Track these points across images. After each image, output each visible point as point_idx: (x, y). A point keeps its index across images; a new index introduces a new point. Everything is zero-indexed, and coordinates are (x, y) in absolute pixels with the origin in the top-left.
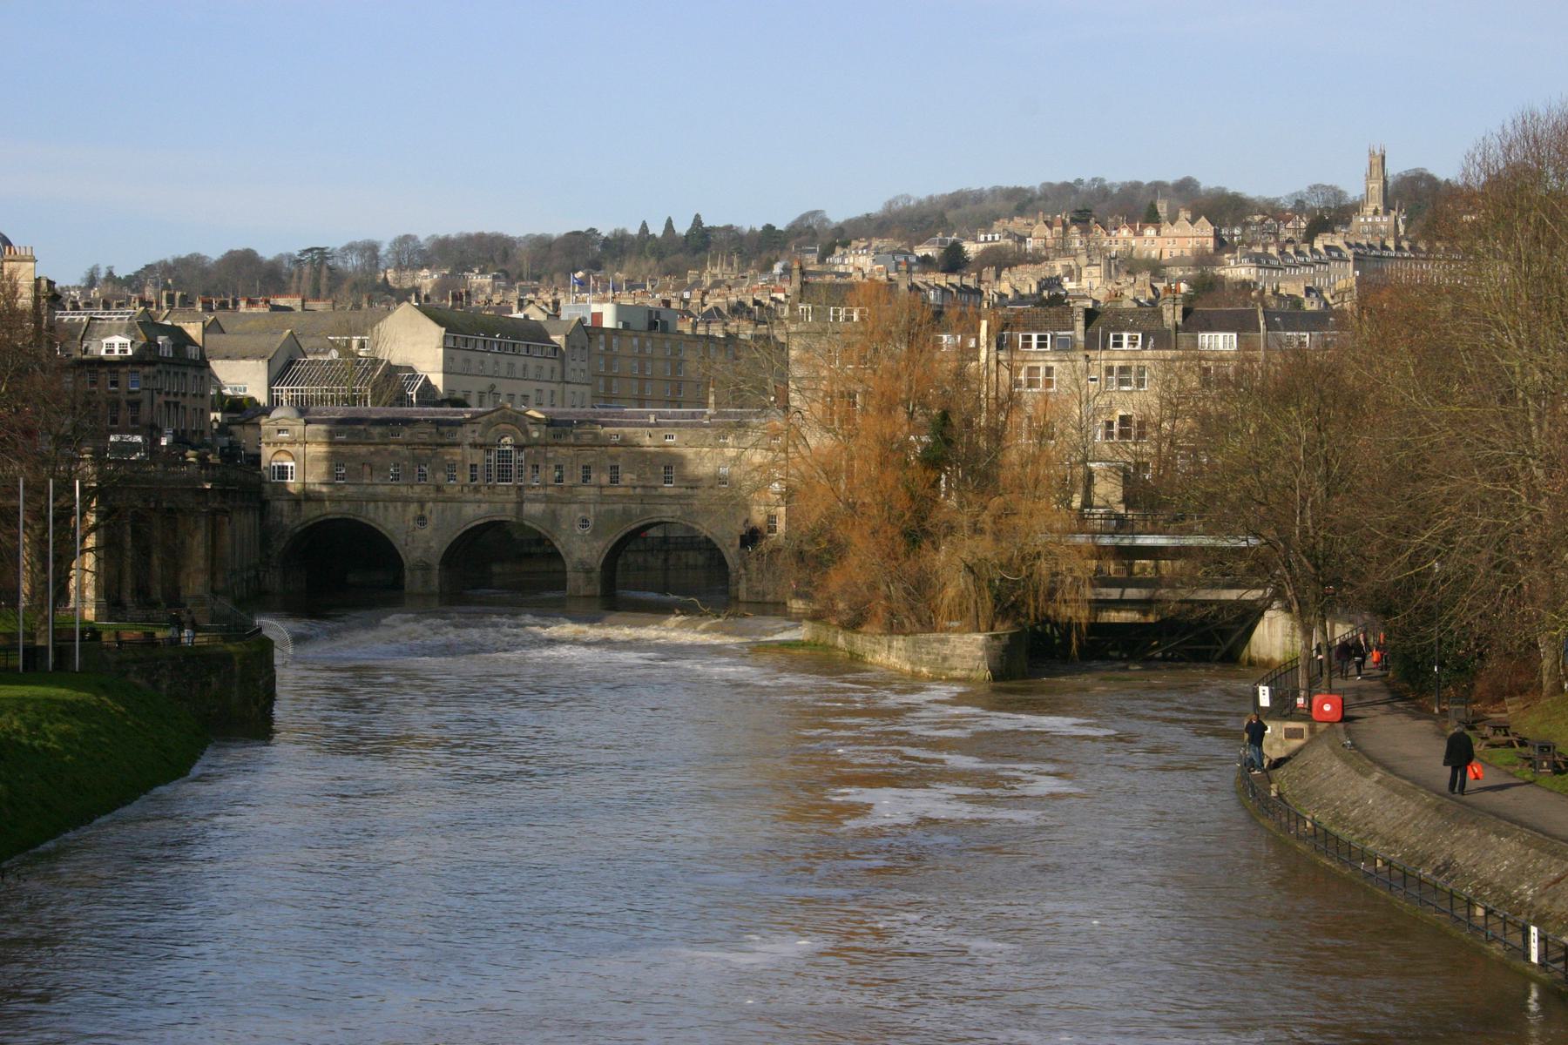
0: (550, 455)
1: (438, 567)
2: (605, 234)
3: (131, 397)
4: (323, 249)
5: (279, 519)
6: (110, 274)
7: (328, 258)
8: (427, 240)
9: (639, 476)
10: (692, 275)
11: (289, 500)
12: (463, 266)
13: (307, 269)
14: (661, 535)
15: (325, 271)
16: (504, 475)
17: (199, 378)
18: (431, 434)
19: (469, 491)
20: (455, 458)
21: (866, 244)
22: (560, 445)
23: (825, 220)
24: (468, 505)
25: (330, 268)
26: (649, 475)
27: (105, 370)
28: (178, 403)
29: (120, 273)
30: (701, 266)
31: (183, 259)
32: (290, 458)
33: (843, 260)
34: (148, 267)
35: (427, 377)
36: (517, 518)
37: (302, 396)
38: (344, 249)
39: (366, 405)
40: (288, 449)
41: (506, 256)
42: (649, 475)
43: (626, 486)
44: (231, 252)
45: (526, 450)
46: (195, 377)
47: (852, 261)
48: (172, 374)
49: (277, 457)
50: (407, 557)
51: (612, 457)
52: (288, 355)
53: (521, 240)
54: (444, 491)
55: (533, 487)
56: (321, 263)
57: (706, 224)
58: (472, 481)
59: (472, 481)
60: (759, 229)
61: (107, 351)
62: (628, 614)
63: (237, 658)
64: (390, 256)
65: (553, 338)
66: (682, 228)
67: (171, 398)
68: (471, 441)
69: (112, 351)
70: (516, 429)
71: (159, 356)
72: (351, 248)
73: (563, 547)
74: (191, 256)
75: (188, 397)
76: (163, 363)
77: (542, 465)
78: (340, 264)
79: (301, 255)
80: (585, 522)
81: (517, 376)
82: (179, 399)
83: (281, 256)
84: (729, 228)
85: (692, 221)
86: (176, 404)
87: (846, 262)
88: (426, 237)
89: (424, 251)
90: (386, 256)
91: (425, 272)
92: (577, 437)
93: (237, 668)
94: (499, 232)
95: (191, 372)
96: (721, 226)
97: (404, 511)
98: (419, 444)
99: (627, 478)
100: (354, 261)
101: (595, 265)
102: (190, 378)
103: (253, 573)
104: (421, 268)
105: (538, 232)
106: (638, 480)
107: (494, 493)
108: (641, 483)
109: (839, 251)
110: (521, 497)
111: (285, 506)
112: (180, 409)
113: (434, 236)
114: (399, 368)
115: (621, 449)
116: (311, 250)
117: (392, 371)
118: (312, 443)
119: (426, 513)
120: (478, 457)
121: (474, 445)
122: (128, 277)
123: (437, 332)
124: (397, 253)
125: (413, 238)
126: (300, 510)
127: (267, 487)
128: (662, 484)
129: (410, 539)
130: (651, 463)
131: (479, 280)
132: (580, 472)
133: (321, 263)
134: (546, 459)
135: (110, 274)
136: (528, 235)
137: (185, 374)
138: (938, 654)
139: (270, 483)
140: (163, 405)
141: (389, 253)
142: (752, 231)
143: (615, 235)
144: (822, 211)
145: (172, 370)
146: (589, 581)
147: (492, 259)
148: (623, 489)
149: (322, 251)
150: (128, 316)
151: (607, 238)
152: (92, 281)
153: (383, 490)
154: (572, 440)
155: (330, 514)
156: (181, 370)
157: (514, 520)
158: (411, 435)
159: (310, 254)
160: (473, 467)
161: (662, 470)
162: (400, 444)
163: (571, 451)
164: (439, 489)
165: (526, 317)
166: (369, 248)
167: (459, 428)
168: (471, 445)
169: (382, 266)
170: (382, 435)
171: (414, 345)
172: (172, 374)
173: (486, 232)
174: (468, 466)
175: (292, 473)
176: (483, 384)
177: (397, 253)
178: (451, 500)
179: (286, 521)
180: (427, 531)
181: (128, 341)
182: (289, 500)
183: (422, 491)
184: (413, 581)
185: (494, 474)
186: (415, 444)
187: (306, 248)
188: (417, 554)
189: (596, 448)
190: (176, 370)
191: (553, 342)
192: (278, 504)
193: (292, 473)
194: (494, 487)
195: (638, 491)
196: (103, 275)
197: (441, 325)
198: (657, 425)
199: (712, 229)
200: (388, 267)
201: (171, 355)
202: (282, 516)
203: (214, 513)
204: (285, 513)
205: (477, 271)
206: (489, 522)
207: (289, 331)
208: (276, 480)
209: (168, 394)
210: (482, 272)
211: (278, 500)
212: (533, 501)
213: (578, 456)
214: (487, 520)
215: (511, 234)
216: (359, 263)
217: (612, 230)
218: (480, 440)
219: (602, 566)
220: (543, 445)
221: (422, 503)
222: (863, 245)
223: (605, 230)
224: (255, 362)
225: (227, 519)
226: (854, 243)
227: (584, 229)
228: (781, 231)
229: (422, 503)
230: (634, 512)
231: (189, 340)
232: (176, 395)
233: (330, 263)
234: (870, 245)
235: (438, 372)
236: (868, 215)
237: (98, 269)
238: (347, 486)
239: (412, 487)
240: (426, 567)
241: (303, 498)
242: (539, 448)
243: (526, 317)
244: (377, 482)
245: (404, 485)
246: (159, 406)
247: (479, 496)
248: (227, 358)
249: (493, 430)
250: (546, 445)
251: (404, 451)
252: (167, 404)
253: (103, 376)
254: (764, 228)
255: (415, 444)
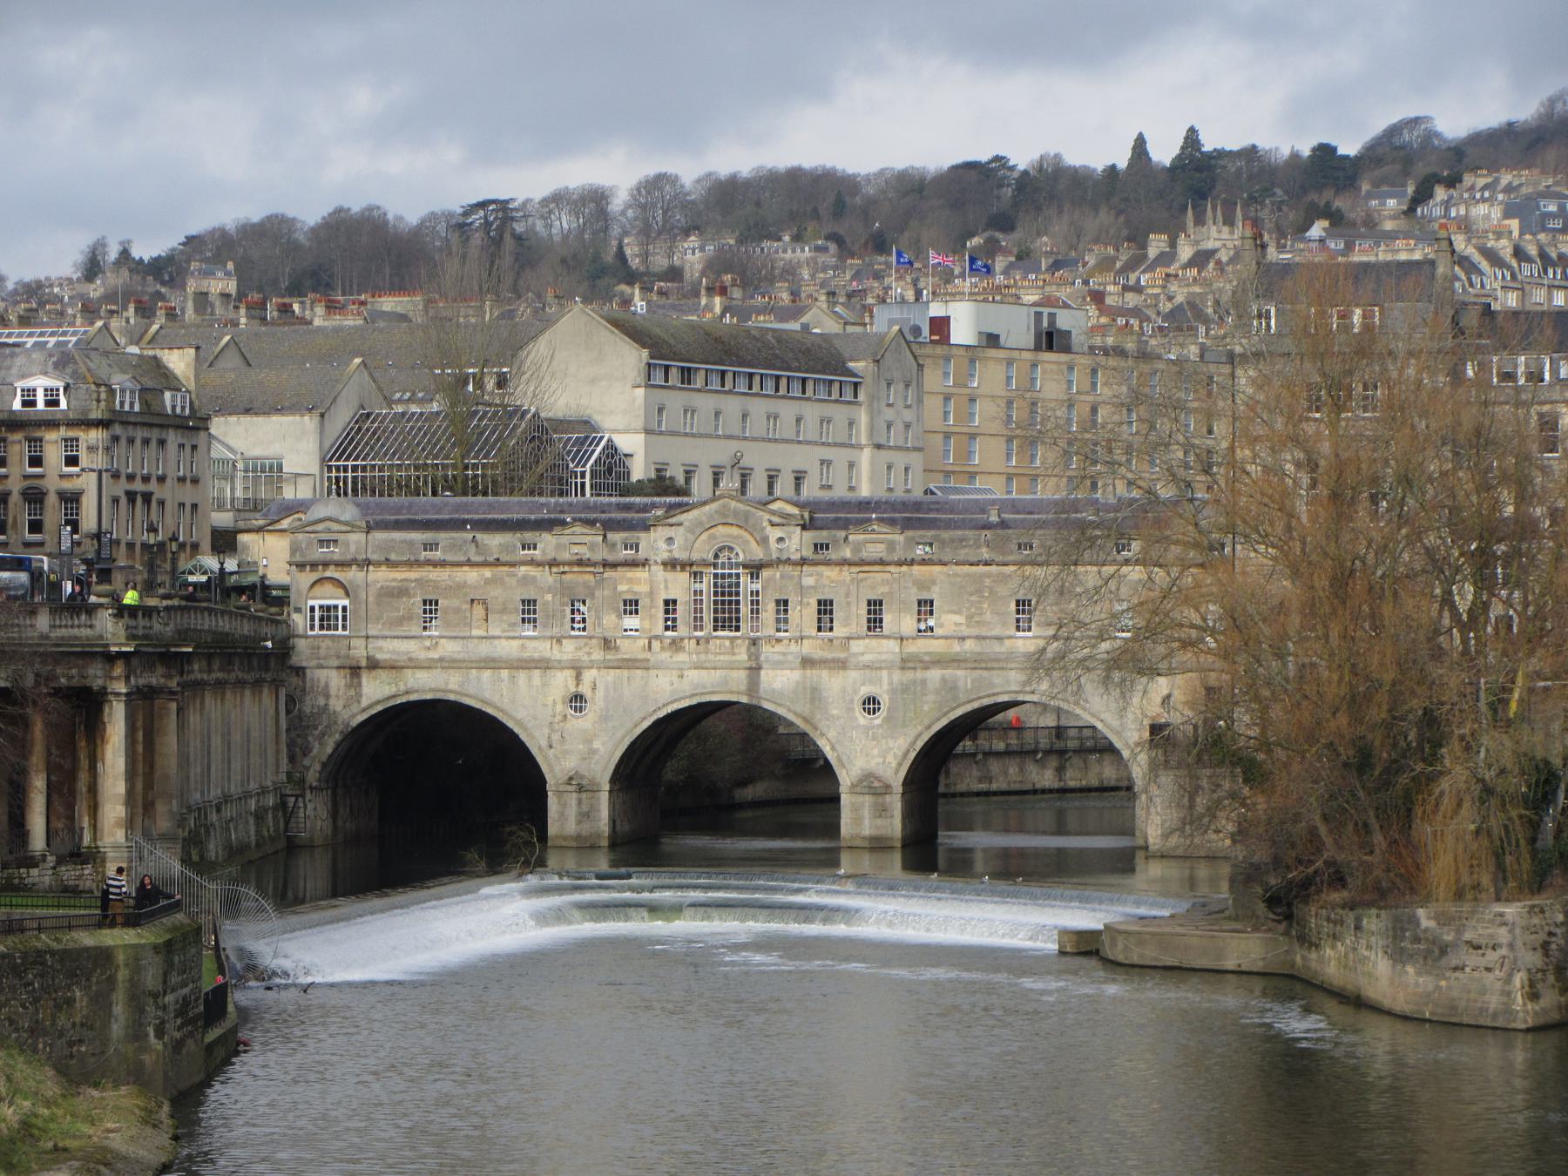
0: (808, 581)
1: (607, 787)
2: (1021, 167)
3: (67, 485)
4: (507, 202)
5: (321, 701)
6: (125, 254)
7: (513, 219)
8: (698, 181)
9: (969, 618)
10: (1156, 244)
11: (338, 668)
12: (759, 231)
13: (477, 239)
14: (1053, 724)
15: (508, 240)
16: (727, 617)
17: (188, 449)
18: (592, 547)
19: (662, 649)
20: (637, 588)
21: (1489, 180)
22: (828, 563)
23: (1431, 135)
24: (660, 673)
25: (518, 238)
26: (988, 616)
27: (18, 436)
28: (151, 494)
29: (144, 251)
30: (1174, 231)
31: (253, 226)
32: (341, 592)
33: (1447, 209)
34: (190, 240)
35: (610, 440)
36: (750, 696)
37: (355, 478)
38: (545, 202)
39: (583, 494)
40: (336, 575)
41: (839, 209)
42: (988, 616)
43: (946, 638)
44: (339, 210)
45: (765, 573)
46: (182, 446)
47: (1463, 212)
48: (138, 442)
49: (318, 590)
50: (552, 770)
51: (922, 585)
52: (356, 404)
53: (867, 178)
54: (616, 649)
55: (779, 640)
56: (501, 230)
57: (1208, 147)
58: (667, 628)
59: (667, 628)
60: (1306, 152)
61: (25, 404)
62: (445, 880)
63: (121, 958)
64: (630, 213)
65: (851, 365)
66: (1164, 152)
67: (138, 486)
68: (665, 556)
69: (33, 403)
70: (746, 535)
71: (114, 411)
72: (557, 199)
73: (833, 748)
74: (269, 218)
75: (169, 481)
76: (122, 423)
77: (793, 601)
78: (539, 226)
79: (466, 214)
80: (871, 704)
81: (785, 436)
82: (153, 486)
83: (433, 216)
84: (1251, 152)
85: (1181, 142)
86: (147, 497)
87: (1453, 214)
88: (695, 176)
89: (693, 202)
90: (623, 213)
91: (693, 241)
92: (857, 548)
93: (122, 975)
94: (829, 164)
95: (173, 438)
96: (1235, 147)
97: (544, 685)
98: (570, 564)
99: (947, 621)
100: (564, 222)
101: (1004, 223)
102: (172, 446)
103: (270, 801)
104: (686, 233)
105: (899, 163)
106: (968, 626)
107: (707, 652)
108: (975, 631)
109: (1440, 193)
110: (757, 658)
111: (335, 681)
112: (154, 504)
113: (709, 174)
114: (562, 424)
115: (938, 568)
116: (483, 205)
117: (541, 431)
118: (378, 564)
119: (585, 689)
120: (678, 586)
121: (671, 564)
122: (157, 260)
123: (633, 358)
124: (643, 207)
125: (672, 180)
126: (360, 684)
127: (301, 644)
128: (1012, 631)
129: (556, 737)
130: (991, 592)
131: (789, 255)
132: (863, 610)
133: (501, 230)
134: (802, 590)
135: (125, 254)
136: (882, 172)
137: (162, 443)
138: (1434, 942)
139: (307, 637)
140: (123, 501)
141: (630, 206)
142: (1295, 156)
143: (1040, 169)
144: (1427, 119)
145: (140, 434)
146: (881, 811)
147: (815, 214)
148: (942, 642)
149: (503, 205)
150: (74, 339)
151: (1025, 173)
152: (92, 268)
153: (508, 648)
154: (847, 553)
155: (451, 691)
156: (155, 434)
157: (744, 700)
158: (558, 547)
159: (482, 213)
160: (670, 604)
161: (1013, 606)
162: (539, 564)
163: (846, 574)
164: (607, 644)
165: (806, 328)
166: (592, 200)
167: (643, 535)
168: (665, 564)
169: (615, 231)
170: (504, 548)
171: (593, 381)
172: (138, 442)
173: (1073, 159)
174: (661, 604)
175: (344, 619)
176: (720, 452)
177: (643, 207)
178: (630, 664)
179: (336, 704)
180: (584, 722)
181: (60, 384)
182: (338, 668)
183: (578, 649)
184: (562, 816)
185: (708, 617)
186: (564, 564)
187: (474, 201)
188: (570, 764)
189: (892, 569)
190: (146, 434)
191: (852, 374)
192: (322, 675)
193: (344, 619)
194: (707, 641)
195: (969, 645)
196: (113, 254)
197: (644, 346)
198: (1003, 524)
199: (1220, 154)
200: (626, 233)
201: (137, 408)
202: (327, 696)
203: (701, 573)
204: (333, 692)
205: (787, 238)
206: (700, 705)
207: (358, 360)
208: (317, 631)
209: (131, 478)
210: (797, 238)
211: (321, 667)
212: (779, 665)
213: (859, 582)
214: (694, 701)
215: (851, 170)
216: (575, 225)
217: (1036, 156)
218: (681, 555)
219: (905, 783)
220: (795, 564)
221: (578, 670)
222: (1481, 182)
223: (1022, 158)
224: (222, 419)
225: (173, 706)
226: (1468, 179)
227: (984, 157)
228: (1346, 157)
229: (578, 670)
230: (961, 684)
231: (168, 379)
232: (146, 479)
233: (519, 228)
234: (1497, 181)
235: (636, 432)
236: (1510, 124)
237: (104, 245)
238: (443, 641)
239: (559, 641)
240: (582, 787)
241: (364, 663)
242: (788, 569)
243: (805, 327)
244: (497, 633)
245: (544, 638)
246: (116, 500)
247: (681, 657)
248: (247, 411)
249: (705, 536)
250: (803, 562)
251: (546, 577)
252: (131, 496)
253: (17, 448)
254: (1314, 150)
255: (564, 564)
